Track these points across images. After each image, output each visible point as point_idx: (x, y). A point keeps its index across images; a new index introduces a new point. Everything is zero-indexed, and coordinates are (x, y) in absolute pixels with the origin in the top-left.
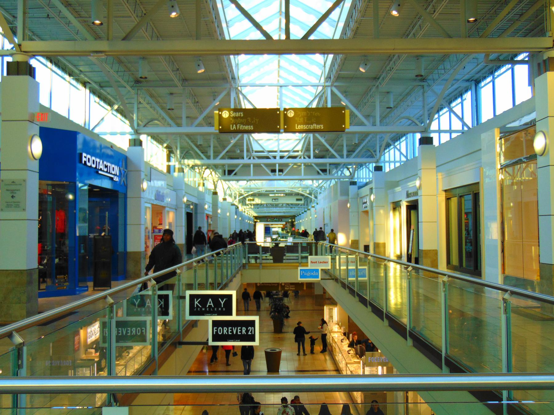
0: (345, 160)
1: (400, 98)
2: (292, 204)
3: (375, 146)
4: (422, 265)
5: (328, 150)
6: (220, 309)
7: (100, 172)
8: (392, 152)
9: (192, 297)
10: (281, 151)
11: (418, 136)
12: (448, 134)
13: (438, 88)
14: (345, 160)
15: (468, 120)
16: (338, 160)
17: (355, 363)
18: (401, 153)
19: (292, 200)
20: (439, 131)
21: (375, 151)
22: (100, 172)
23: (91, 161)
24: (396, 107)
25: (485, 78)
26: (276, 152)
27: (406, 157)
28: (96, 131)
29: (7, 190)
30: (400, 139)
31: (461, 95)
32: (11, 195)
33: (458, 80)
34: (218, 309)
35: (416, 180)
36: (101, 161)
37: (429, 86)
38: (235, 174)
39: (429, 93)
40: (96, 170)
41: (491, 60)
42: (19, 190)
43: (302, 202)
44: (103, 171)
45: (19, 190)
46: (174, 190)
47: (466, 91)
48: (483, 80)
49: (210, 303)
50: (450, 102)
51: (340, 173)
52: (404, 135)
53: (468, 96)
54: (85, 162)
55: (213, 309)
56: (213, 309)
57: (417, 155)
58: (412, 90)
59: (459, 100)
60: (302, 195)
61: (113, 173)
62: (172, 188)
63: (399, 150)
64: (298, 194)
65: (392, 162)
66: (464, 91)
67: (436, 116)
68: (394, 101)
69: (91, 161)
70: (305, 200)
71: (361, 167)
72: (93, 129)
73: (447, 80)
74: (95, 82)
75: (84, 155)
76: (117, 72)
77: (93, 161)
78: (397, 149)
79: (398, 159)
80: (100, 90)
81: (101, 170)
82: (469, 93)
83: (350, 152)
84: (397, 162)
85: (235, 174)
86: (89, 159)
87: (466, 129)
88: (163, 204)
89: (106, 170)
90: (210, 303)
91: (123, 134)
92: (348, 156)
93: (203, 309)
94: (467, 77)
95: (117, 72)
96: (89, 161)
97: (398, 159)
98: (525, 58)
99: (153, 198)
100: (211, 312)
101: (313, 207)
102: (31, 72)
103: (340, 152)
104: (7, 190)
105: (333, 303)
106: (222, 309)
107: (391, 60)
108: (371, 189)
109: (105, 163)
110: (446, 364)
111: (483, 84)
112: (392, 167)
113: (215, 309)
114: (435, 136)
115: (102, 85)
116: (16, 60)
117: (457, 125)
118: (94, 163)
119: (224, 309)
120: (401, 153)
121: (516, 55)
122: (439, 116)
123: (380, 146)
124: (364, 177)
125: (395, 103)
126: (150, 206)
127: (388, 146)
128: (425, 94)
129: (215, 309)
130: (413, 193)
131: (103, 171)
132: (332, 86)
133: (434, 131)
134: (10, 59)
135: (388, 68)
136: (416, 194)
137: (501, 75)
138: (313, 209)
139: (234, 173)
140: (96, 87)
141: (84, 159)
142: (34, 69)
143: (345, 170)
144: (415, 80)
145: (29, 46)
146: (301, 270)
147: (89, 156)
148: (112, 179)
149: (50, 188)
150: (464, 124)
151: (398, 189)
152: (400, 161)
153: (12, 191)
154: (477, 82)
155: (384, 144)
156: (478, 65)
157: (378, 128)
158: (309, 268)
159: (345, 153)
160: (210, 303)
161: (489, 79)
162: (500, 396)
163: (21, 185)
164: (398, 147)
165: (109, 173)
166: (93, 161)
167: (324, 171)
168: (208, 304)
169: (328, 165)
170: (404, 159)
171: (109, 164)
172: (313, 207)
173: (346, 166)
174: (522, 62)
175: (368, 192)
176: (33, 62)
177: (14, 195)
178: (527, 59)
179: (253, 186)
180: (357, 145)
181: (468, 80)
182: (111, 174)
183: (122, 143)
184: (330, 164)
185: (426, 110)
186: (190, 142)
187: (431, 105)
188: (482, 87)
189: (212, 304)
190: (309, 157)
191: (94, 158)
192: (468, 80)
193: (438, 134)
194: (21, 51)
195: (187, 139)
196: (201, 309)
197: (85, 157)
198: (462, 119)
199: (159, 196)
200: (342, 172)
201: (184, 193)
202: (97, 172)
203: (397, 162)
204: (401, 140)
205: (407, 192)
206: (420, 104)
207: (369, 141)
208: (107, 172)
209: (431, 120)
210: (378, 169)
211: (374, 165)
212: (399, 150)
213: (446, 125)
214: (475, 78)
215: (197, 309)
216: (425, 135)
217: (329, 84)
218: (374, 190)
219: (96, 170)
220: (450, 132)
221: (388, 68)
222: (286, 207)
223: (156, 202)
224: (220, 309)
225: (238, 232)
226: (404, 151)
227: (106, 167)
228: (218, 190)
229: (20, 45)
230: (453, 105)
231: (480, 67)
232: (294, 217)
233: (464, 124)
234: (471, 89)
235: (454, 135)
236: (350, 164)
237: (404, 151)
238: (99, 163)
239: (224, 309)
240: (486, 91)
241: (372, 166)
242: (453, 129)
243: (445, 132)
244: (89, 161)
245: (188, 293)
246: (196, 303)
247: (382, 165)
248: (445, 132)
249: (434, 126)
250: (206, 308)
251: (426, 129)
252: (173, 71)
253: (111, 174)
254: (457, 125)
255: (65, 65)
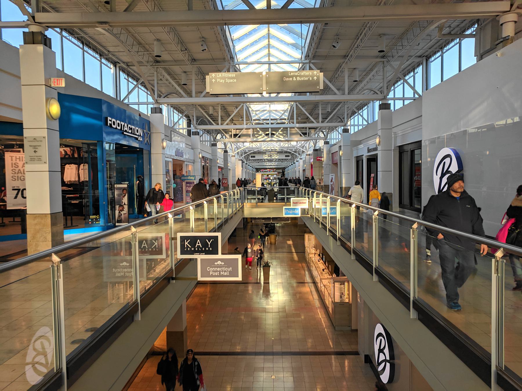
0: (320, 125)
1: (364, 74)
2: (282, 159)
3: (343, 114)
4: (392, 211)
5: (308, 118)
6: (207, 249)
7: (125, 133)
8: (356, 118)
9: (183, 239)
10: (272, 120)
11: (377, 104)
12: (402, 101)
13: (396, 64)
14: (320, 125)
15: (419, 88)
16: (315, 125)
17: (328, 278)
18: (363, 118)
19: (283, 157)
20: (394, 99)
21: (344, 118)
22: (125, 133)
23: (116, 124)
24: (361, 81)
25: (435, 53)
26: (268, 120)
27: (367, 121)
28: (126, 101)
29: (30, 146)
30: (362, 108)
31: (414, 70)
32: (34, 150)
33: (412, 56)
34: (205, 249)
35: (376, 138)
36: (126, 124)
37: (388, 61)
38: (239, 137)
39: (388, 68)
40: (121, 131)
41: (444, 35)
42: (40, 146)
43: (290, 158)
44: (128, 132)
45: (40, 146)
46: (192, 149)
47: (418, 66)
48: (433, 55)
49: (199, 243)
50: (405, 76)
51: (316, 135)
52: (366, 105)
53: (420, 70)
54: (110, 124)
55: (202, 249)
56: (202, 249)
57: (376, 118)
58: (375, 66)
59: (412, 74)
60: (290, 153)
61: (137, 134)
62: (190, 147)
63: (362, 116)
64: (286, 152)
65: (356, 125)
66: (416, 66)
67: (392, 88)
68: (359, 76)
69: (116, 124)
70: (290, 155)
71: (332, 130)
72: (123, 101)
73: (402, 57)
74: (124, 62)
75: (109, 118)
76: (138, 52)
77: (118, 124)
78: (361, 115)
79: (360, 123)
80: (123, 67)
81: (126, 131)
82: (421, 67)
83: (324, 119)
84: (360, 125)
85: (239, 137)
86: (114, 122)
87: (416, 96)
88: (182, 159)
89: (130, 131)
90: (199, 244)
91: (147, 104)
92: (322, 122)
93: (193, 249)
94: (419, 54)
95: (138, 52)
96: (114, 124)
97: (360, 123)
98: (473, 32)
99: (174, 154)
100: (200, 252)
101: (297, 161)
102: (47, 42)
103: (316, 118)
104: (30, 146)
105: (310, 232)
106: (209, 248)
107: (358, 39)
108: (340, 147)
109: (129, 126)
110: (414, 307)
111: (433, 58)
112: (356, 130)
113: (203, 249)
114: (391, 102)
115: (129, 64)
116: (31, 31)
117: (409, 93)
118: (119, 126)
119: (211, 249)
120: (363, 118)
121: (464, 31)
122: (394, 88)
123: (348, 114)
124: (356, 123)
125: (361, 77)
126: (171, 160)
127: (354, 113)
128: (385, 68)
129: (203, 249)
130: (373, 149)
131: (128, 132)
132: (310, 62)
133: (391, 99)
134: (152, 106)
135: (356, 46)
136: (375, 149)
137: (449, 49)
138: (297, 163)
139: (238, 136)
140: (124, 66)
141: (109, 122)
142: (50, 39)
143: (321, 133)
144: (377, 57)
145: (41, 17)
146: (285, 209)
147: (113, 120)
148: (137, 139)
149: (86, 146)
150: (415, 92)
151: (361, 146)
152: (363, 125)
153: (35, 147)
154: (428, 58)
155: (350, 112)
156: (431, 40)
157: (346, 97)
158: (292, 207)
159: (320, 119)
160: (199, 244)
161: (439, 54)
162: (486, 361)
163: (41, 141)
164: (361, 114)
165: (134, 134)
166: (118, 124)
167: (305, 134)
168: (197, 244)
169: (308, 129)
170: (365, 123)
171: (133, 127)
172: (297, 161)
173: (321, 129)
174: (471, 36)
175: (338, 150)
176: (50, 33)
177: (36, 150)
178: (474, 33)
179: (254, 146)
180: (329, 113)
181: (420, 56)
182: (136, 135)
183: (145, 110)
184: (309, 128)
185: (385, 83)
186: (203, 112)
187: (390, 78)
188: (432, 62)
189: (200, 244)
190: (293, 123)
191: (118, 122)
192: (420, 56)
193: (405, 96)
194: (36, 23)
195: (200, 109)
196: (191, 249)
197: (110, 120)
198: (413, 88)
199: (179, 153)
200: (318, 135)
201: (199, 151)
202: (123, 133)
203: (360, 125)
204: (396, 85)
205: (368, 148)
206: (381, 77)
207: (339, 110)
208: (131, 133)
209: (347, 121)
210: (346, 131)
211: (342, 128)
212: (362, 116)
213: (401, 94)
214: (425, 54)
215: (187, 249)
216: (385, 102)
217: (307, 61)
218: (342, 147)
219: (121, 131)
220: (403, 99)
221: (356, 46)
222: (278, 161)
223: (176, 158)
224: (207, 249)
225: (243, 180)
226: (365, 117)
227: (131, 129)
228: (228, 149)
229: (33, 17)
230: (407, 78)
231: (431, 43)
232: (284, 168)
233: (415, 92)
234: (422, 64)
235: (407, 102)
236: (325, 128)
237: (365, 117)
238: (124, 126)
239: (211, 249)
240: (435, 65)
241: (340, 129)
242: (405, 96)
243: (399, 99)
244: (114, 124)
245: (179, 235)
246: (186, 243)
247: (349, 128)
248: (399, 99)
249: (391, 95)
250: (195, 248)
251: (385, 98)
252: (182, 51)
253: (136, 135)
254: (409, 93)
255: (95, 47)
